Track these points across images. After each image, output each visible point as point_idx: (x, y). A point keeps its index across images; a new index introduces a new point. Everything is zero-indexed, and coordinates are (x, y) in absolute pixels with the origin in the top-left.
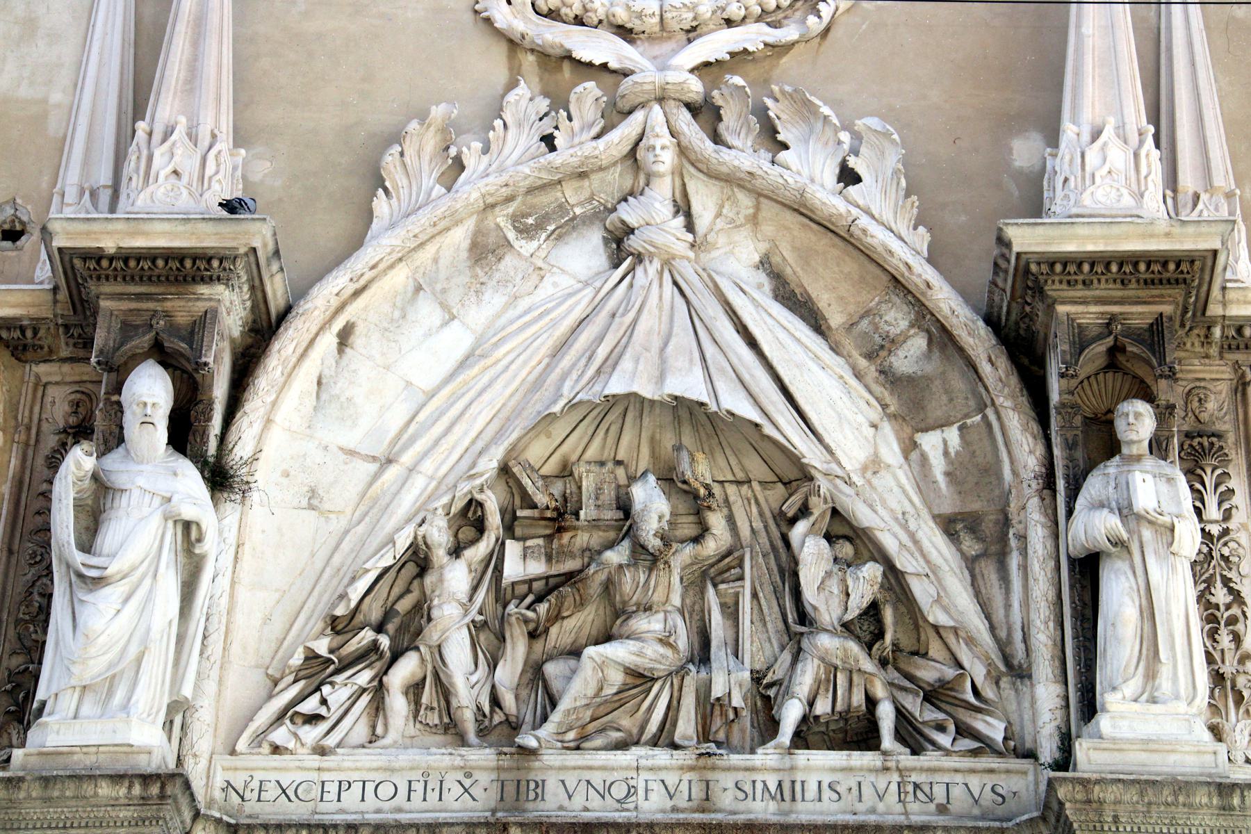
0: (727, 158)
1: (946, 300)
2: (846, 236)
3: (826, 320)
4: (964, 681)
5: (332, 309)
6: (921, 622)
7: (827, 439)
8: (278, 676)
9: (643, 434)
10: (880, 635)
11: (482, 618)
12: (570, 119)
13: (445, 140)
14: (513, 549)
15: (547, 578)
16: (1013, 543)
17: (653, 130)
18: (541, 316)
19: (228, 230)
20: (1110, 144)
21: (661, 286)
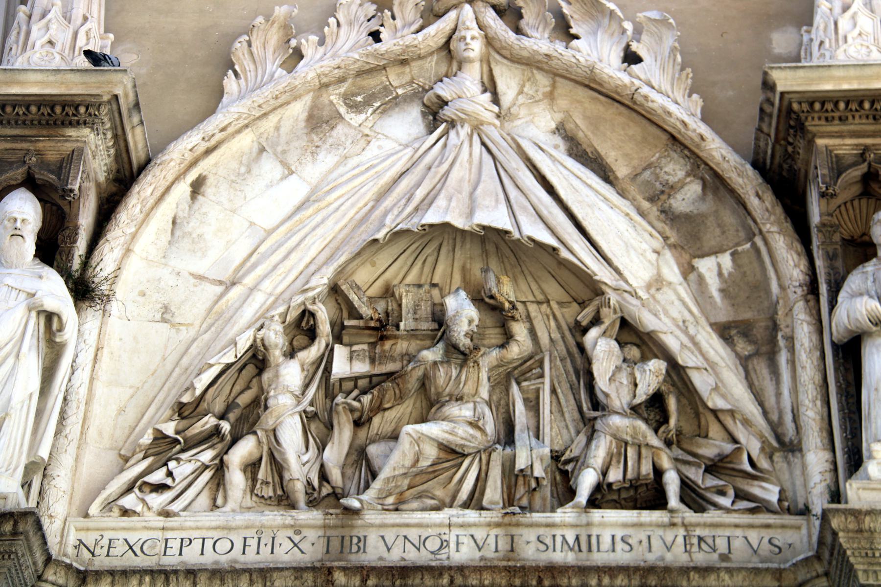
0: (527, 43)
1: (717, 149)
2: (630, 104)
3: (613, 172)
4: (741, 454)
5: (186, 163)
6: (701, 409)
7: (616, 262)
8: (129, 454)
9: (456, 264)
10: (666, 420)
11: (312, 409)
12: (393, 18)
13: (287, 35)
14: (340, 352)
15: (371, 377)
16: (782, 343)
17: (464, 23)
18: (368, 169)
19: (93, 80)
20: (860, 13)
21: (471, 146)
